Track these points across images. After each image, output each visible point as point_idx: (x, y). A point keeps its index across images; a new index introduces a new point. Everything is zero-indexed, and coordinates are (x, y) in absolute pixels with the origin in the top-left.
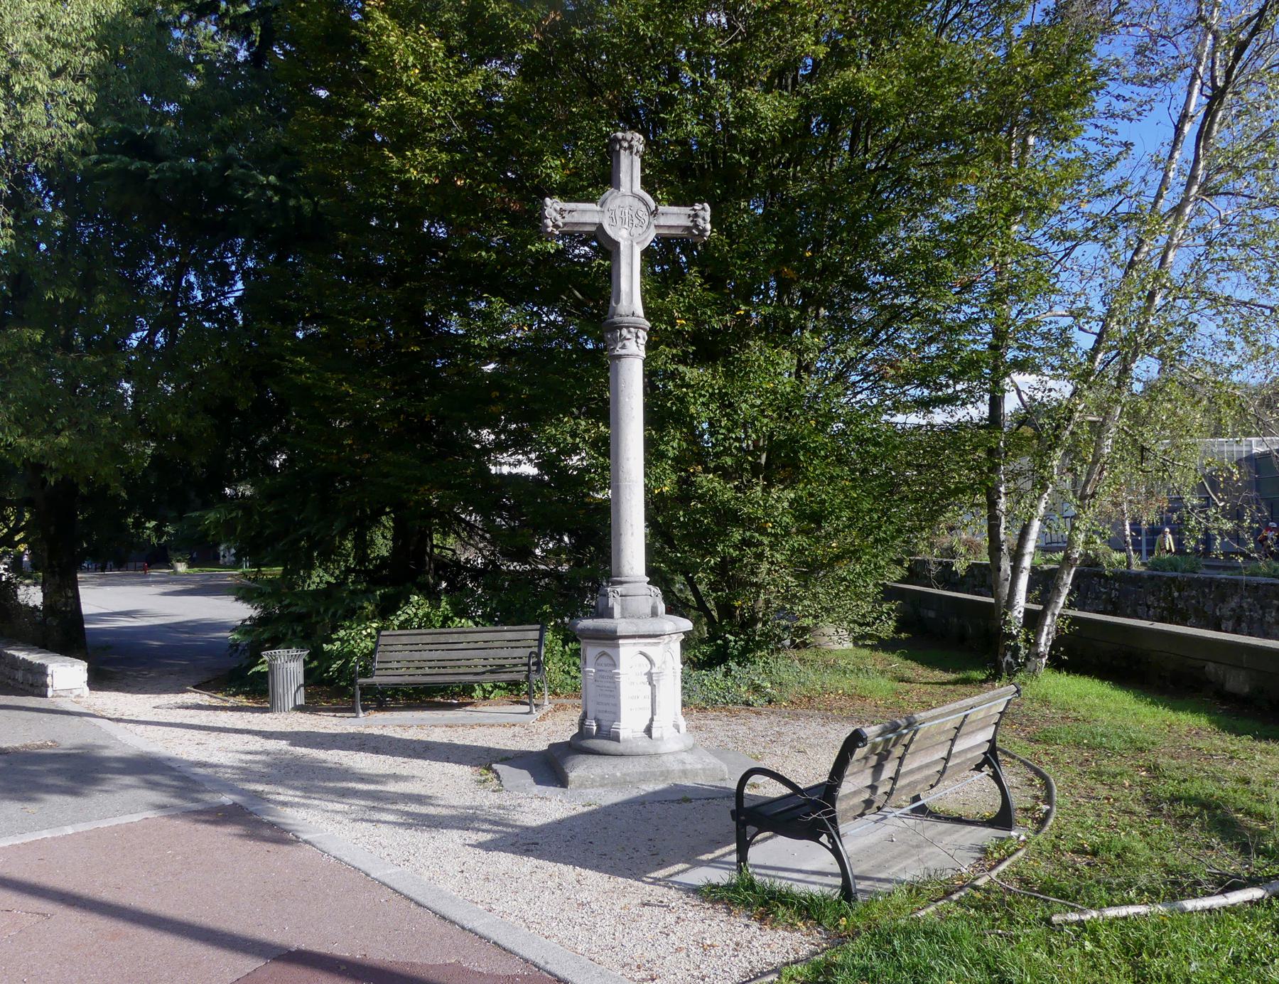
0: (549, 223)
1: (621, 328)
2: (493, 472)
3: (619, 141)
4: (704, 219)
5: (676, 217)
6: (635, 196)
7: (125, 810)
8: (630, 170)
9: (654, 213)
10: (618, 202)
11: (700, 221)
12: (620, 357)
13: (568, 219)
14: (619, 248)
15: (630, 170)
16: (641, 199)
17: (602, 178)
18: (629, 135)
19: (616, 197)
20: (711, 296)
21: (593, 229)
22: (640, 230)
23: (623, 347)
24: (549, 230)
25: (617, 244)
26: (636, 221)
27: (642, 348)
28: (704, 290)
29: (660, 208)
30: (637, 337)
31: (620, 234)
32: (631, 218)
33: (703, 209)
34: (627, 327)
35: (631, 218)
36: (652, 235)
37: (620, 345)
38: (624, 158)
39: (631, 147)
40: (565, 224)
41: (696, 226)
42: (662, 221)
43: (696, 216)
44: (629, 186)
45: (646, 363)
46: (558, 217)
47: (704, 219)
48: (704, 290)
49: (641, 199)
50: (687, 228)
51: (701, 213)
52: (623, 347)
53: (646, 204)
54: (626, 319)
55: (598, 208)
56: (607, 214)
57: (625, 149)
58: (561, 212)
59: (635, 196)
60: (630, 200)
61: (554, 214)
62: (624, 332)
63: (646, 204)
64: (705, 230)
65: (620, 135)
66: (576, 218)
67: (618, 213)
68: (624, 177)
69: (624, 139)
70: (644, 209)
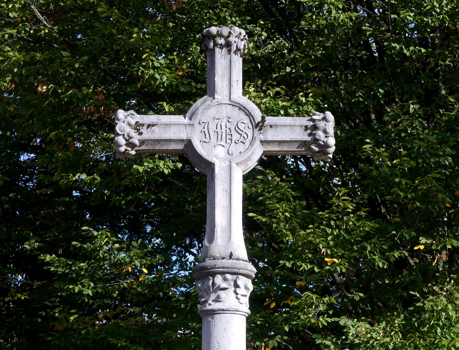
0: (121, 140)
1: (214, 275)
2: (74, 194)
3: (212, 37)
4: (325, 132)
5: (288, 130)
6: (234, 104)
7: (173, 128)
8: (228, 71)
9: (259, 126)
10: (212, 112)
11: (320, 135)
12: (213, 313)
13: (147, 134)
14: (213, 170)
15: (228, 71)
16: (243, 109)
17: (189, 90)
18: (225, 31)
19: (209, 107)
20: (369, 226)
21: (180, 147)
22: (241, 148)
23: (218, 300)
24: (122, 149)
25: (210, 166)
26: (236, 136)
27: (246, 300)
28: (359, 218)
29: (269, 120)
30: (236, 286)
31: (213, 152)
32: (229, 131)
33: (324, 119)
34: (222, 273)
35: (229, 131)
36: (257, 152)
37: (213, 296)
38: (221, 57)
39: (228, 45)
40: (142, 142)
41: (316, 141)
42: (270, 135)
43: (315, 128)
44: (226, 92)
45: (250, 320)
46: (133, 133)
47: (325, 132)
48: (359, 218)
49: (243, 109)
50: (304, 143)
51: (321, 124)
52: (218, 300)
53: (249, 115)
54: (219, 263)
55: (187, 121)
56: (198, 128)
57: (221, 47)
58: (138, 127)
59: (234, 104)
60: (228, 110)
61: (128, 130)
62: (219, 279)
63: (249, 115)
64: (327, 146)
65: (214, 30)
66: (157, 133)
67: (212, 127)
68: (220, 81)
69: (220, 35)
70: (246, 120)
